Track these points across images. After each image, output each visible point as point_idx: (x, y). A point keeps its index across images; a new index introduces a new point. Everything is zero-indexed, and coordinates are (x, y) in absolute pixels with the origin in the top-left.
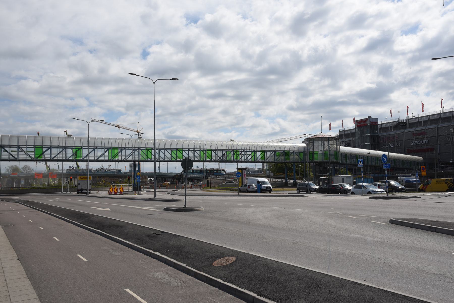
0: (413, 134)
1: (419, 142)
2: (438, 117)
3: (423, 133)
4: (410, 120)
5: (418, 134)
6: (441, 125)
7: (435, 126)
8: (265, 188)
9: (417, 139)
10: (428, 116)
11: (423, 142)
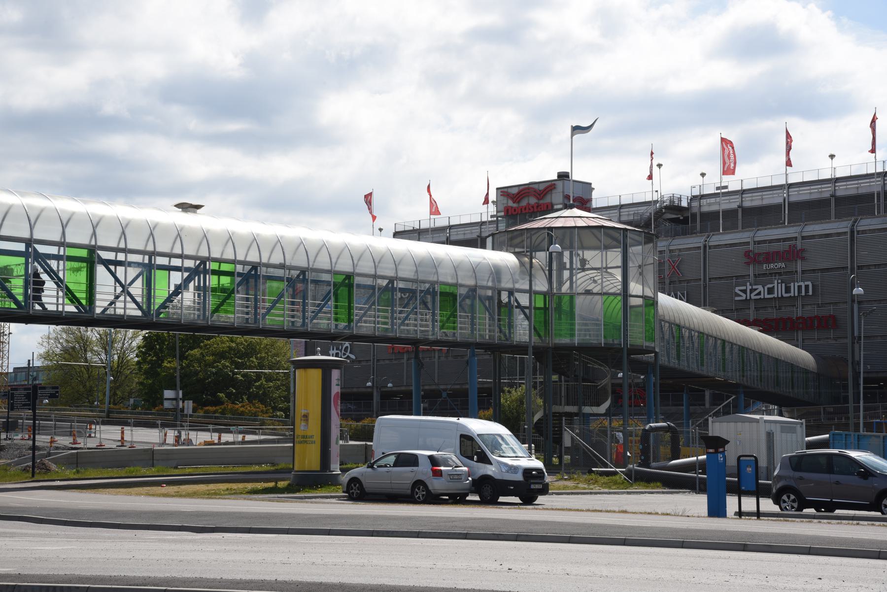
0: (747, 254)
1: (771, 291)
2: (827, 195)
3: (792, 253)
4: (704, 202)
5: (770, 257)
6: (866, 224)
7: (842, 226)
8: (519, 477)
9: (760, 278)
10: (780, 187)
11: (788, 290)
